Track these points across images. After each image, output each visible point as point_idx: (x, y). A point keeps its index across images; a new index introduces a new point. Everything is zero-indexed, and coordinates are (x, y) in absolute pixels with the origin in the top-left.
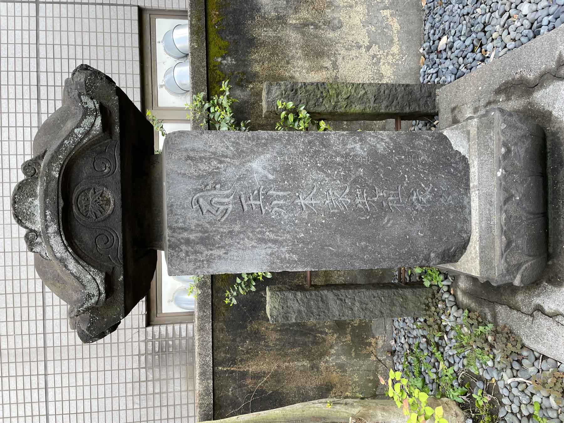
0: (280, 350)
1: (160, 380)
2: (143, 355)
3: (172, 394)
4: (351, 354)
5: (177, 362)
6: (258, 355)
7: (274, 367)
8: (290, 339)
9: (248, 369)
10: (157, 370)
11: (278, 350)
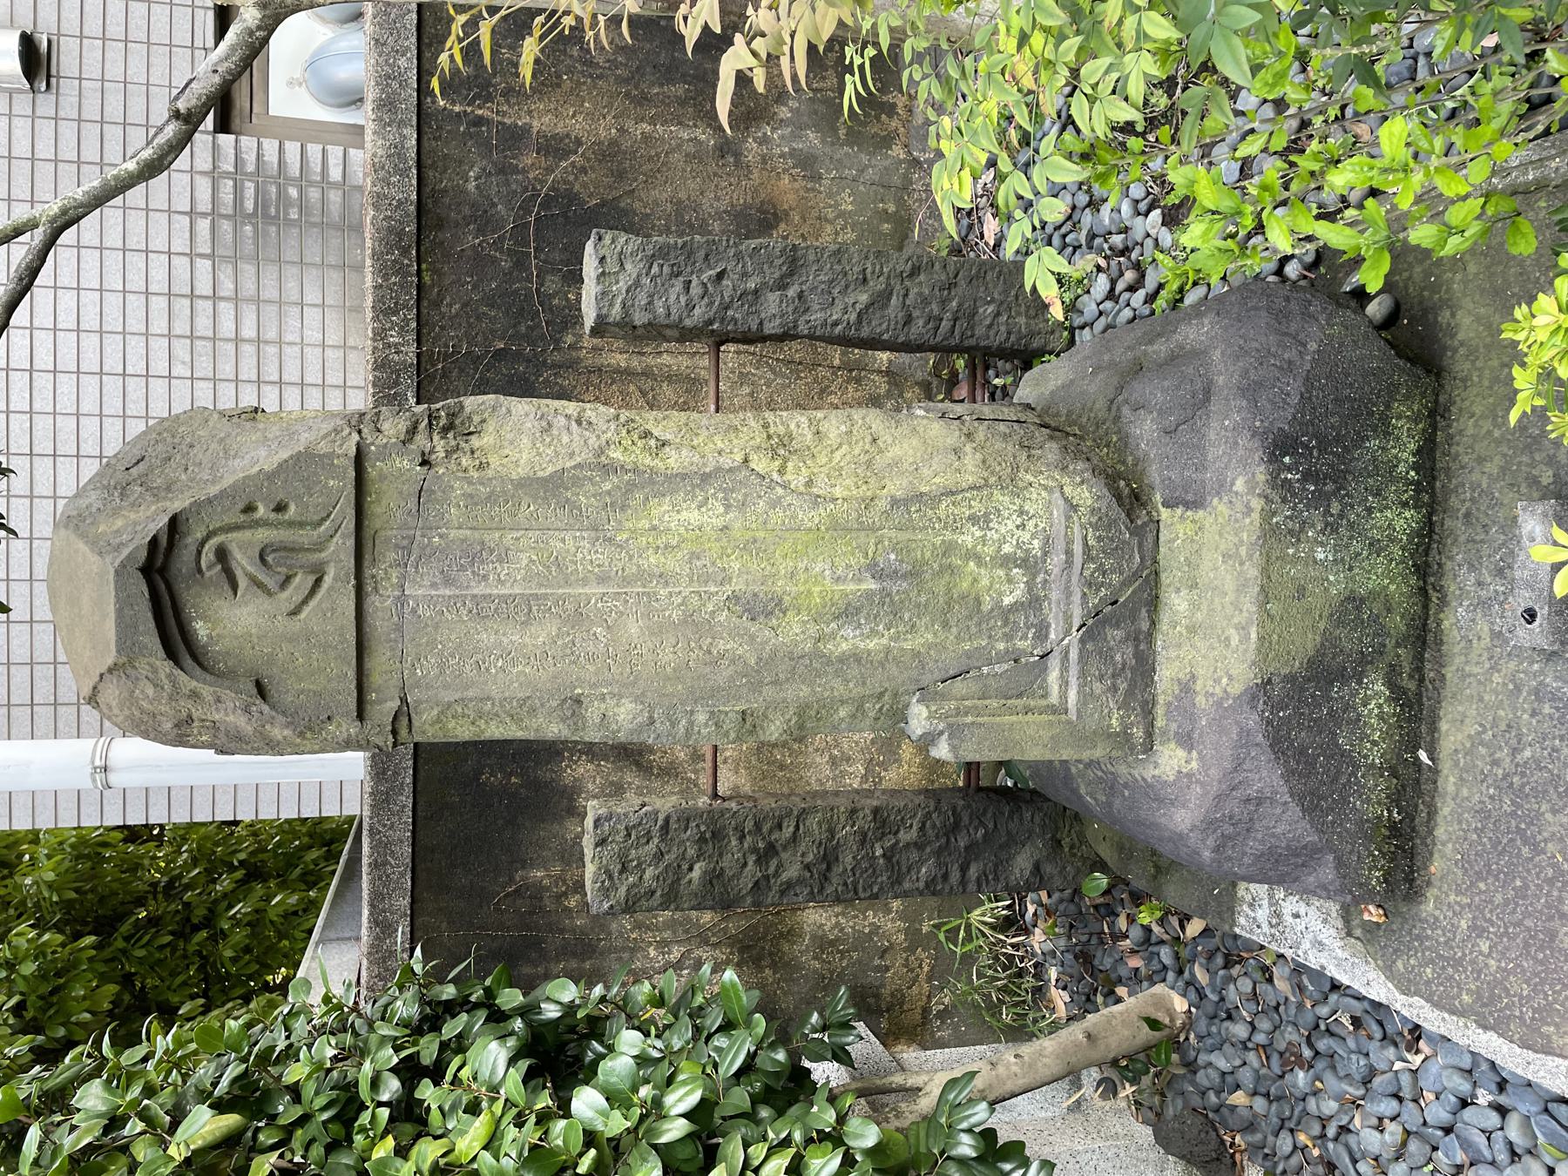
0: (627, 81)
1: (257, 301)
2: (204, 215)
3: (297, 349)
4: (835, 130)
5: (313, 254)
6: (559, 86)
7: (606, 130)
8: (658, 54)
9: (528, 119)
10: (248, 270)
11: (621, 81)
